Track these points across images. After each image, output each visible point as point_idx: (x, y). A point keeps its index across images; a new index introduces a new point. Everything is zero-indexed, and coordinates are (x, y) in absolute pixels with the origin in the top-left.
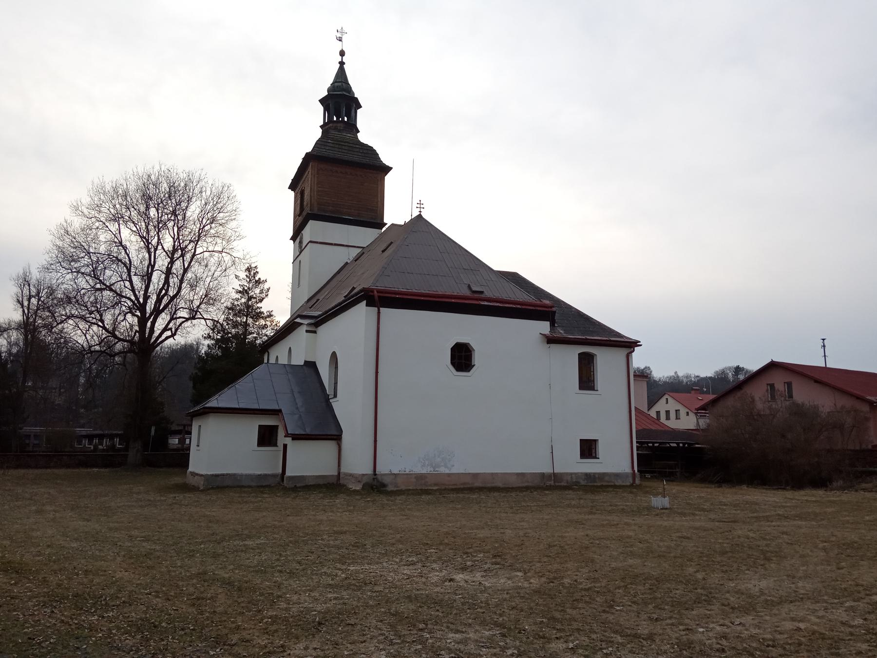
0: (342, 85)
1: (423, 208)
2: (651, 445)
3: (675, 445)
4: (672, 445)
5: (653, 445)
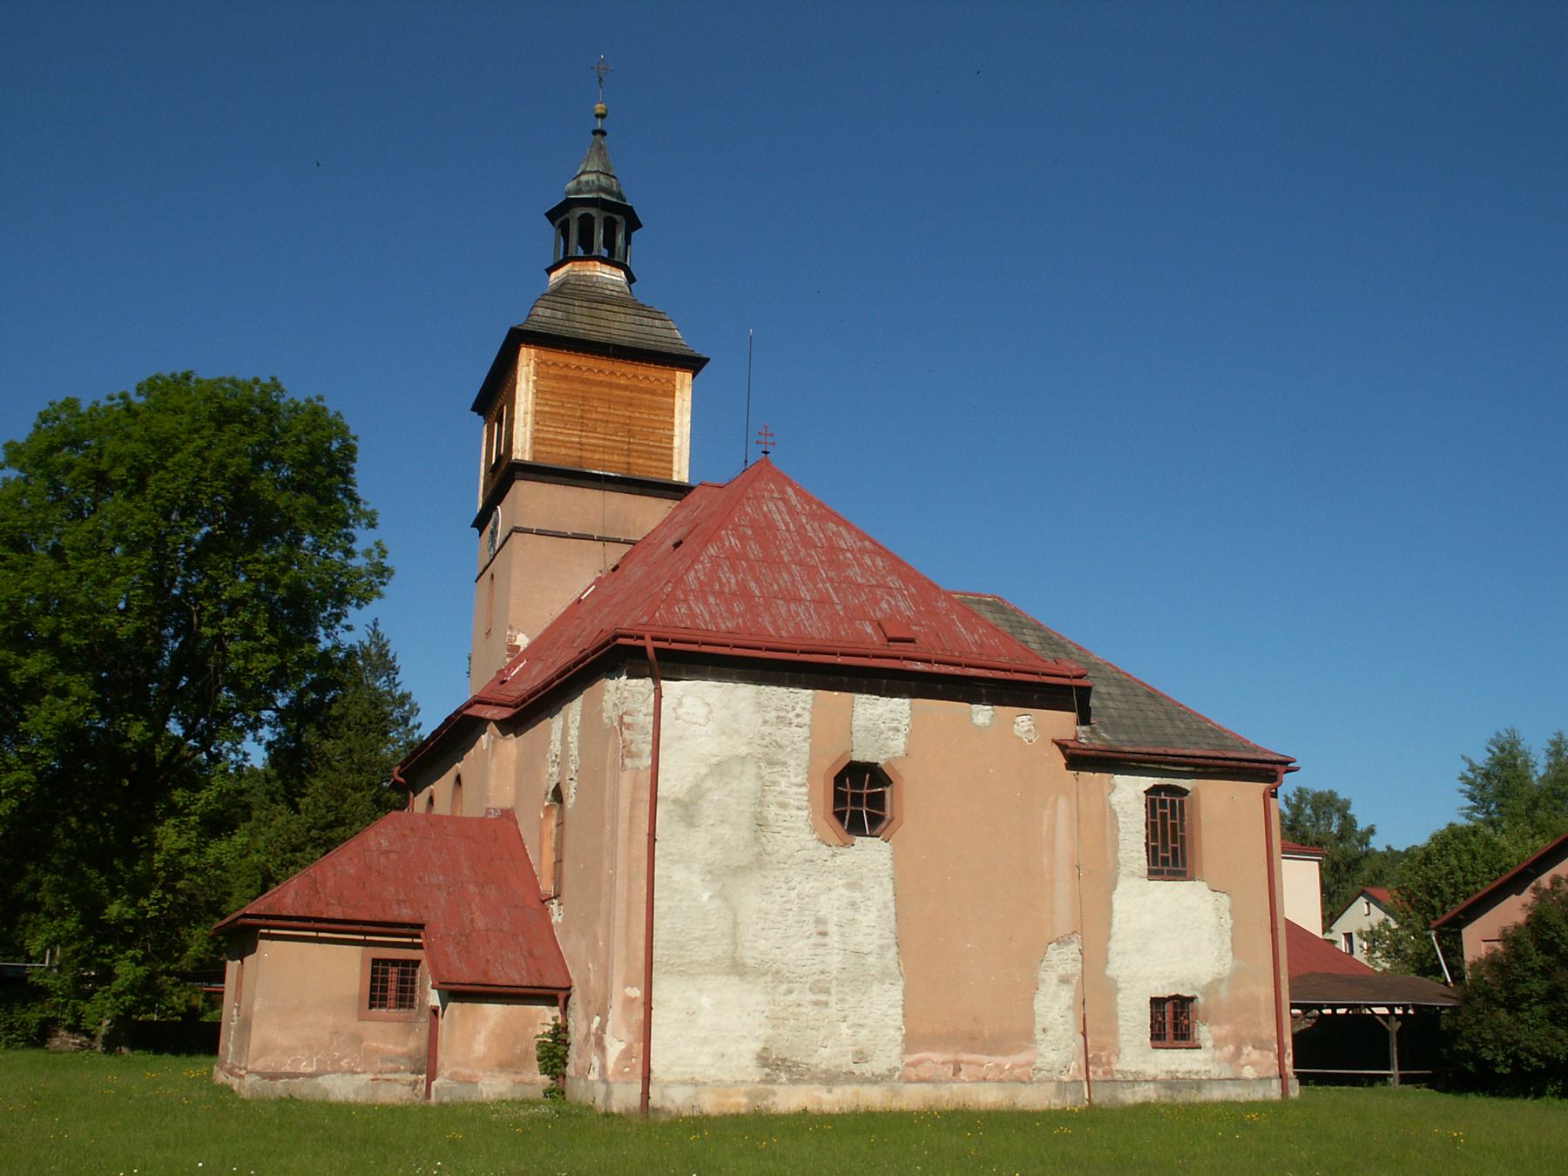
0: (598, 179)
1: (774, 444)
2: (1328, 1011)
3: (1385, 1011)
4: (1377, 1010)
5: (1334, 1011)
